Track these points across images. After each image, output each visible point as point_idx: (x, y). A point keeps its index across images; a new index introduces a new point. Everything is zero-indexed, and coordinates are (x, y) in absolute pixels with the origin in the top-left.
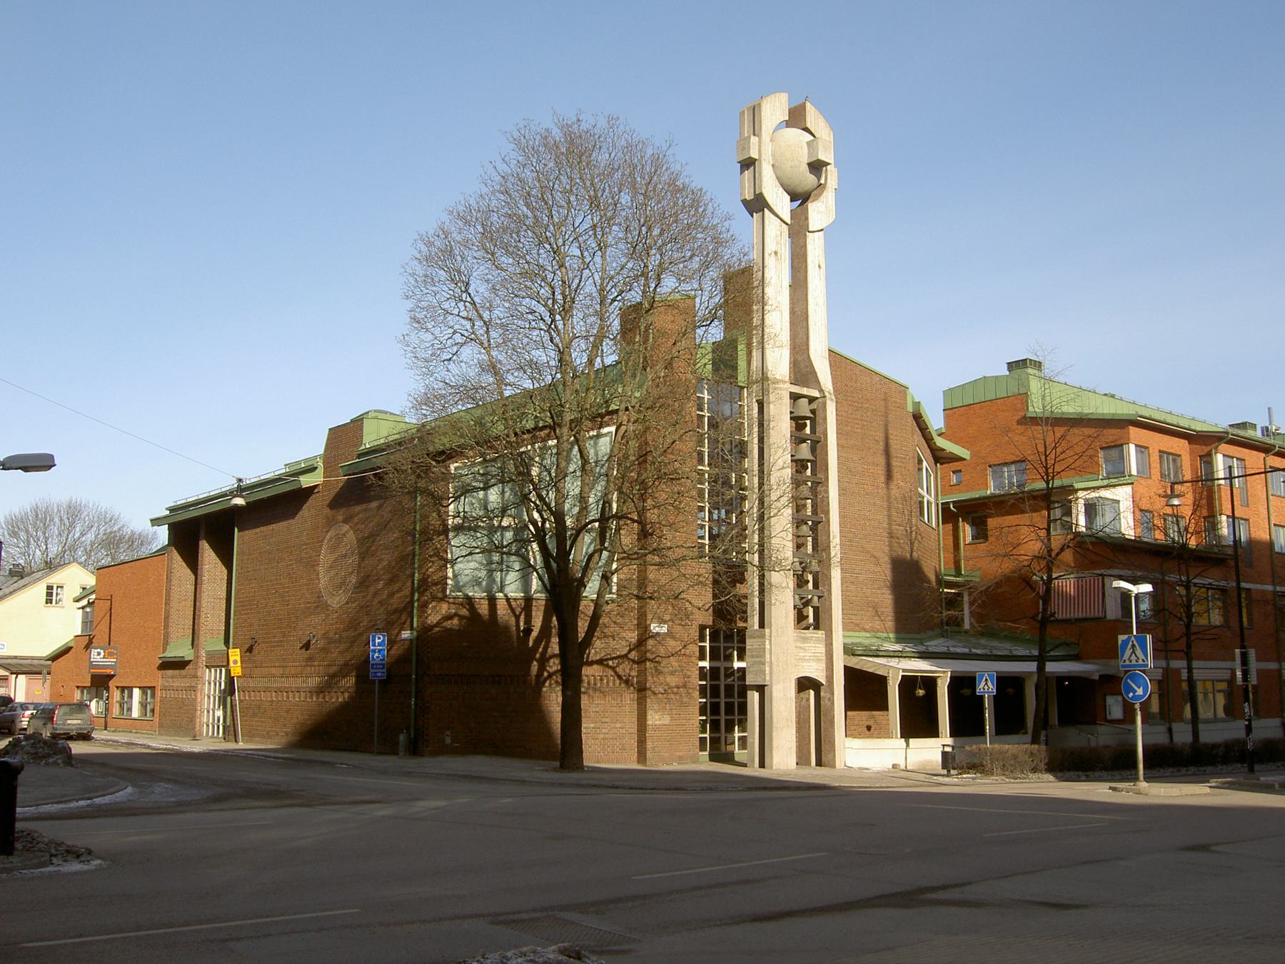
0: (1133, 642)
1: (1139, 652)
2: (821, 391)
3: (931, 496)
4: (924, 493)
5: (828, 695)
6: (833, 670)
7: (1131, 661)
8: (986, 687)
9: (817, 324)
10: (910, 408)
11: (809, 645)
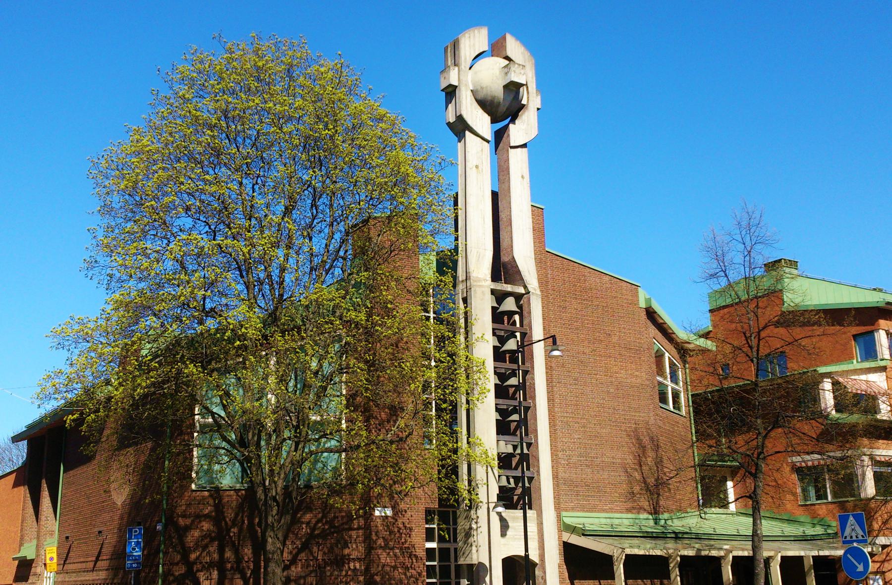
3: (677, 383)
6: (544, 549)
10: (643, 304)
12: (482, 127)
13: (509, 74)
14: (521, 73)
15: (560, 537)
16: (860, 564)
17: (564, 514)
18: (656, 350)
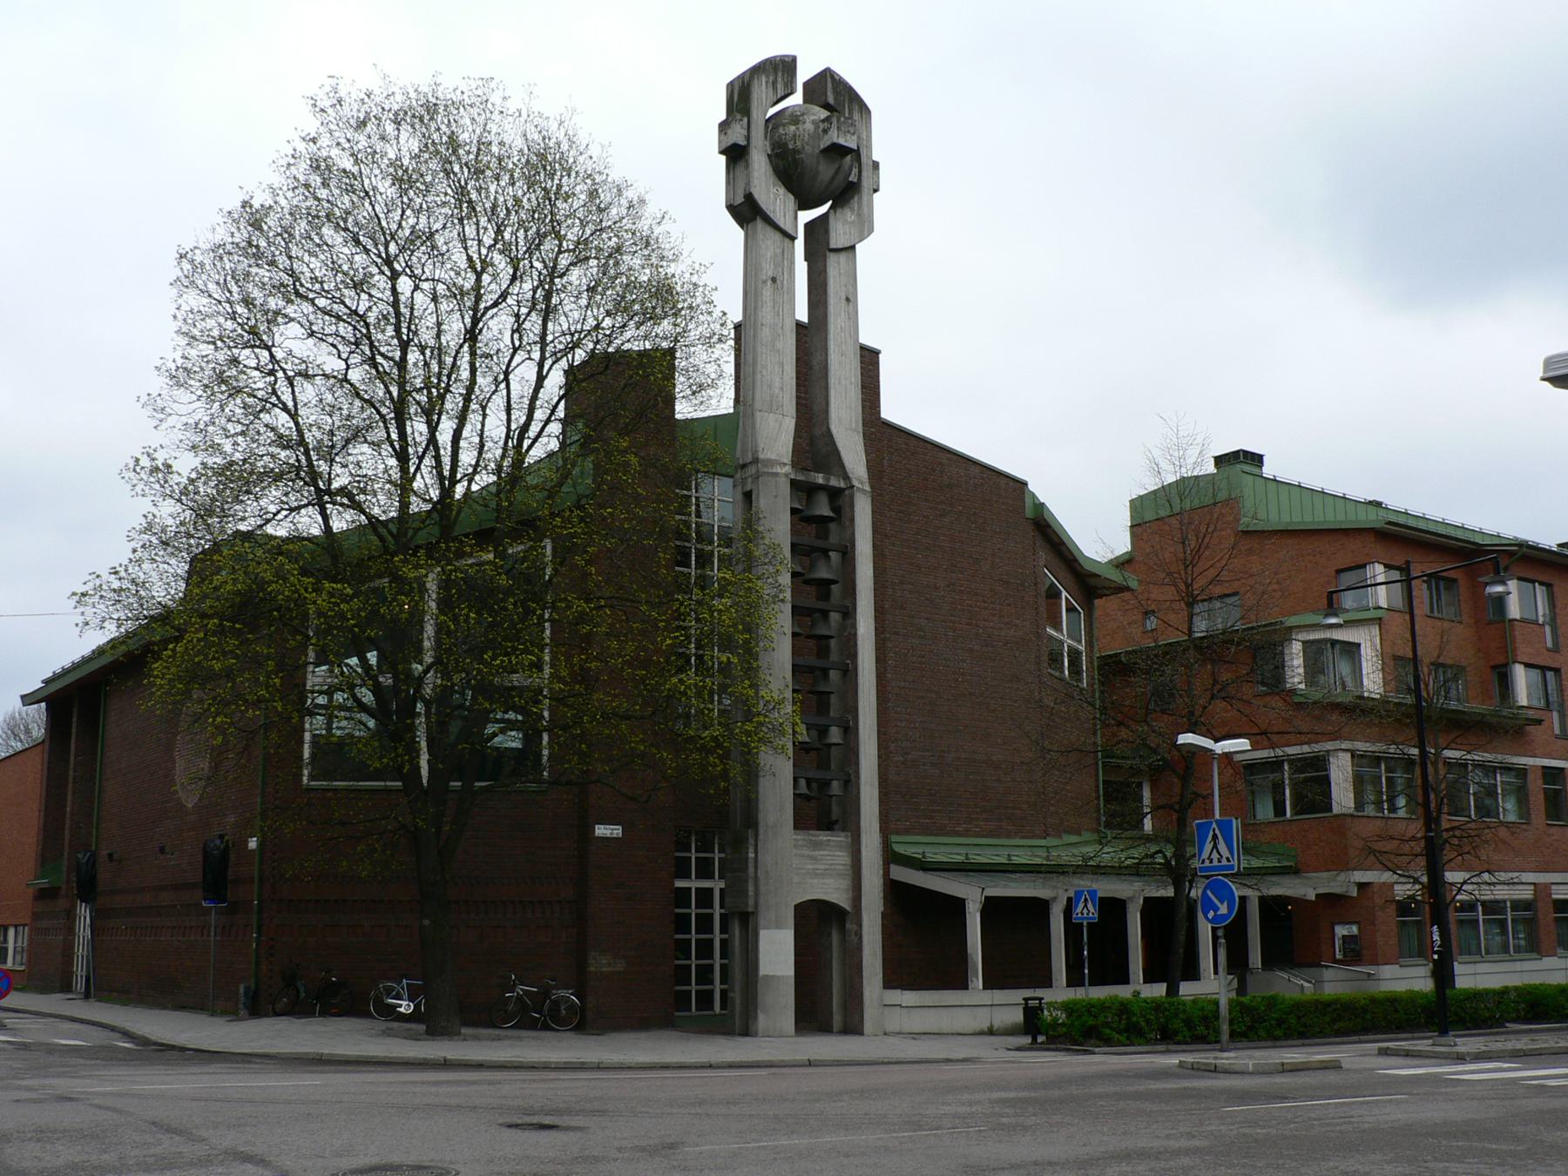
0: (1214, 830)
1: (1222, 846)
2: (846, 477)
4: (1063, 636)
5: (855, 927)
7: (1211, 862)
8: (1085, 911)
9: (843, 382)
11: (822, 853)
12: (785, 216)
13: (830, 133)
14: (849, 132)
15: (886, 873)
16: (1222, 903)
17: (894, 838)
18: (1047, 586)
